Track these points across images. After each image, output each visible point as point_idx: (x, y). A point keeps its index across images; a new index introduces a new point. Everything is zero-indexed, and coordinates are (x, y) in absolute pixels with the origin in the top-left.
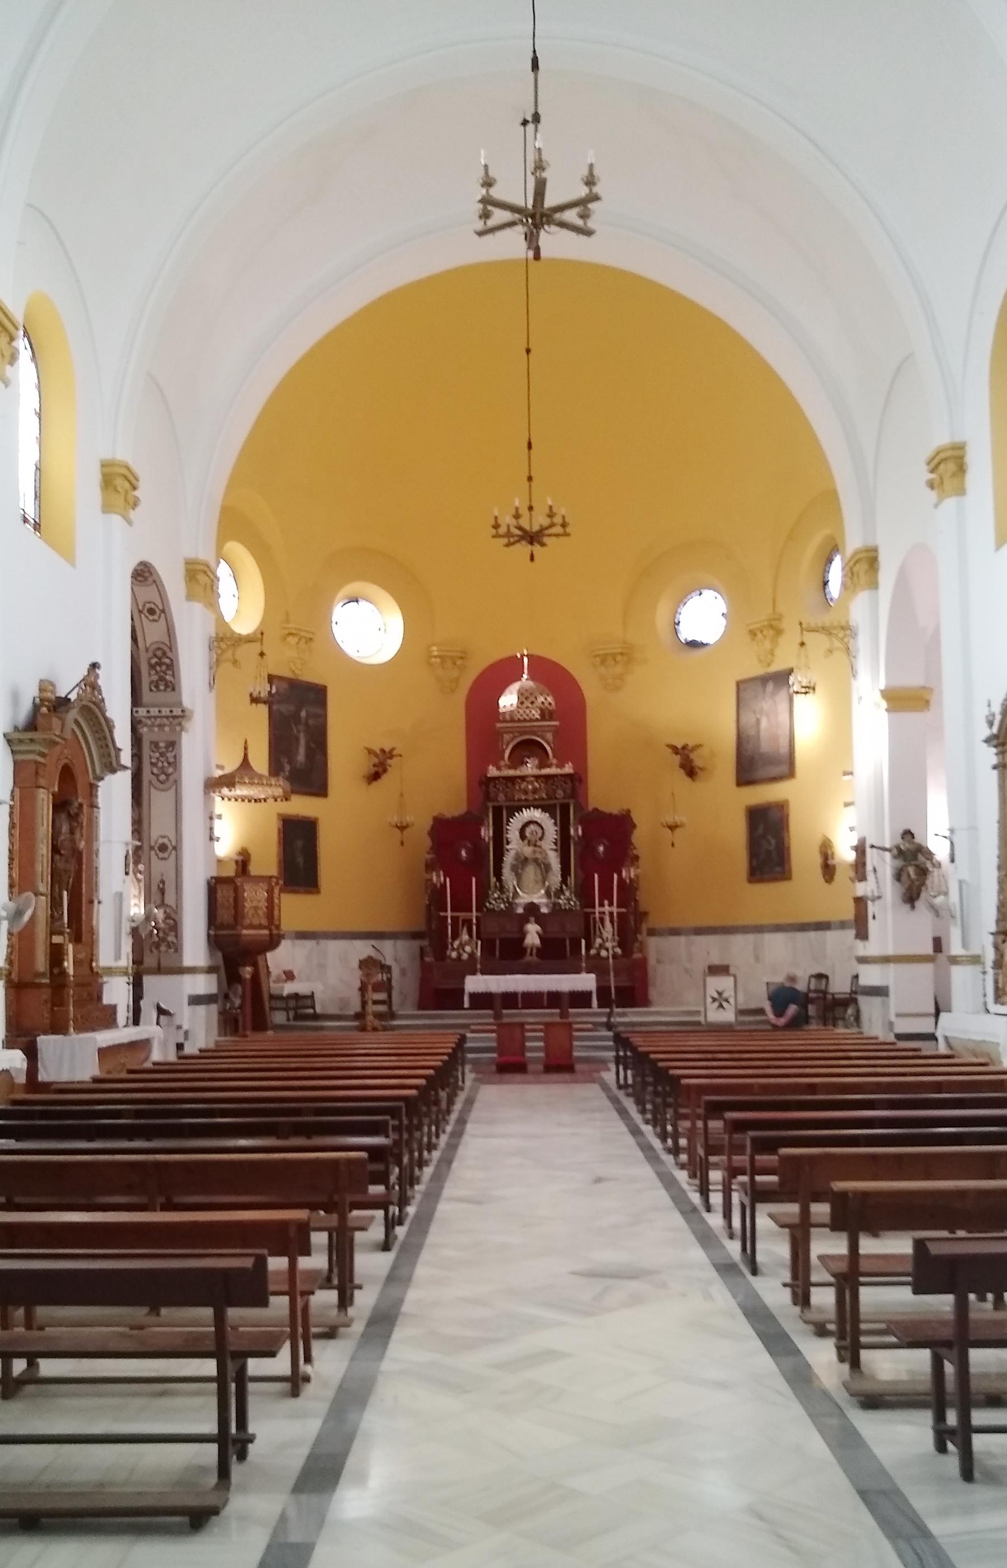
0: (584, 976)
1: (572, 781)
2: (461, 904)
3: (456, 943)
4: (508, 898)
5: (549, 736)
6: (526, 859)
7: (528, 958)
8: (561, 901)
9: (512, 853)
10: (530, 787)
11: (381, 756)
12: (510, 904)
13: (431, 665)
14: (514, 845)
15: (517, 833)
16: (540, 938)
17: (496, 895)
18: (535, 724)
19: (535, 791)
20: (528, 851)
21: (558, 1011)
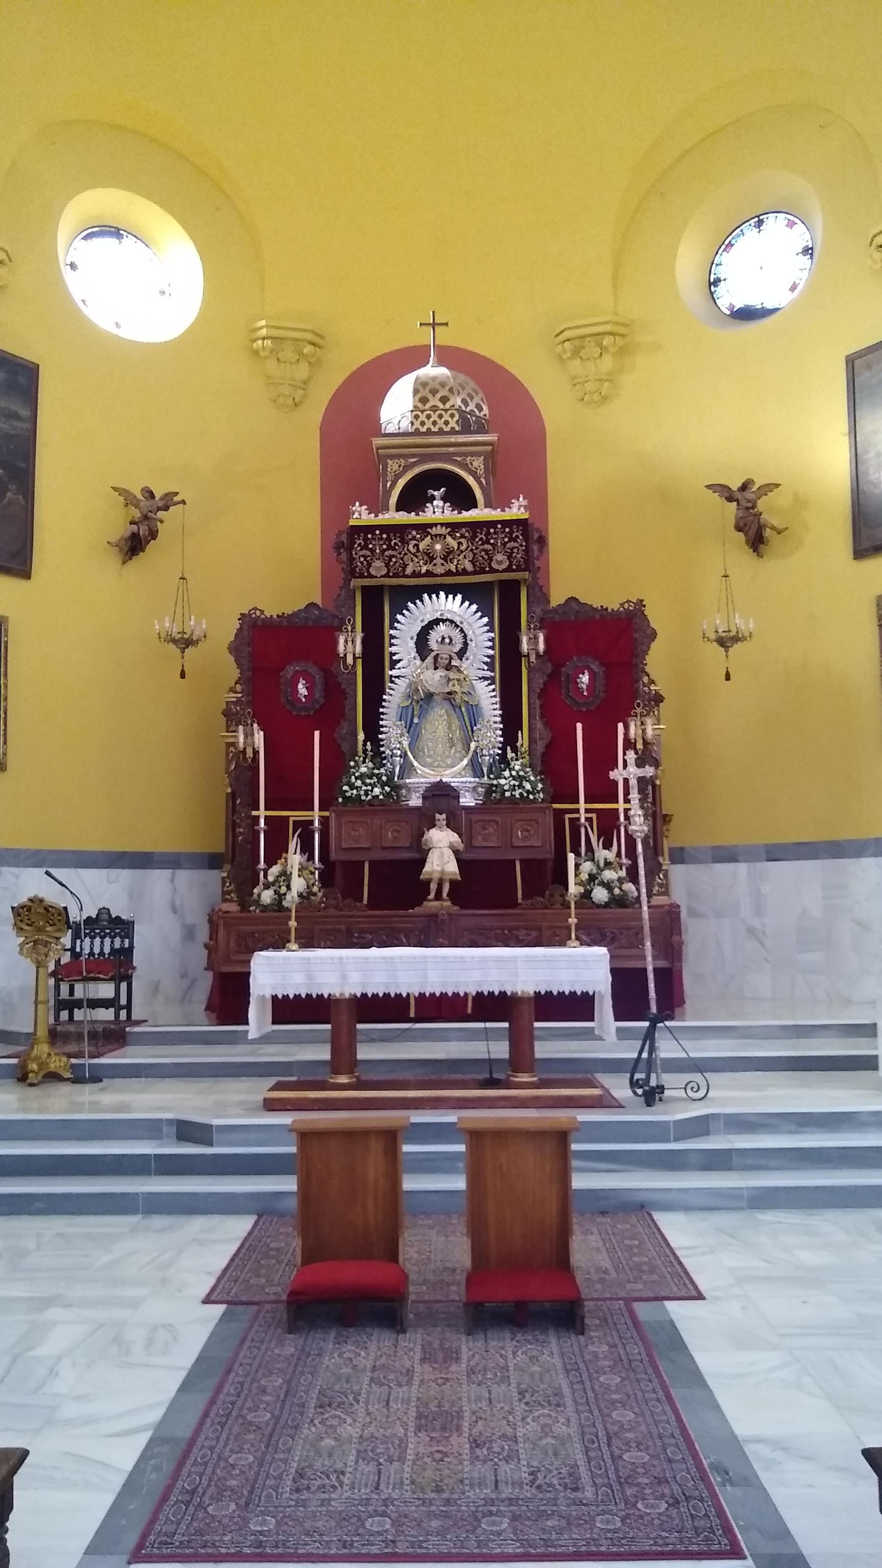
0: (574, 951)
1: (526, 537)
2: (289, 790)
3: (275, 870)
4: (391, 778)
5: (478, 463)
6: (430, 696)
7: (431, 905)
8: (502, 781)
9: (401, 685)
10: (438, 547)
11: (145, 504)
12: (396, 788)
13: (256, 353)
14: (407, 669)
15: (412, 644)
16: (459, 861)
17: (363, 769)
18: (453, 439)
19: (448, 555)
20: (433, 679)
21: (506, 1025)
